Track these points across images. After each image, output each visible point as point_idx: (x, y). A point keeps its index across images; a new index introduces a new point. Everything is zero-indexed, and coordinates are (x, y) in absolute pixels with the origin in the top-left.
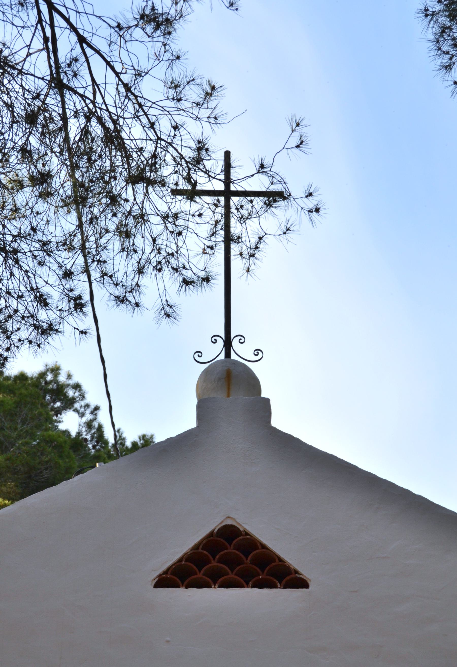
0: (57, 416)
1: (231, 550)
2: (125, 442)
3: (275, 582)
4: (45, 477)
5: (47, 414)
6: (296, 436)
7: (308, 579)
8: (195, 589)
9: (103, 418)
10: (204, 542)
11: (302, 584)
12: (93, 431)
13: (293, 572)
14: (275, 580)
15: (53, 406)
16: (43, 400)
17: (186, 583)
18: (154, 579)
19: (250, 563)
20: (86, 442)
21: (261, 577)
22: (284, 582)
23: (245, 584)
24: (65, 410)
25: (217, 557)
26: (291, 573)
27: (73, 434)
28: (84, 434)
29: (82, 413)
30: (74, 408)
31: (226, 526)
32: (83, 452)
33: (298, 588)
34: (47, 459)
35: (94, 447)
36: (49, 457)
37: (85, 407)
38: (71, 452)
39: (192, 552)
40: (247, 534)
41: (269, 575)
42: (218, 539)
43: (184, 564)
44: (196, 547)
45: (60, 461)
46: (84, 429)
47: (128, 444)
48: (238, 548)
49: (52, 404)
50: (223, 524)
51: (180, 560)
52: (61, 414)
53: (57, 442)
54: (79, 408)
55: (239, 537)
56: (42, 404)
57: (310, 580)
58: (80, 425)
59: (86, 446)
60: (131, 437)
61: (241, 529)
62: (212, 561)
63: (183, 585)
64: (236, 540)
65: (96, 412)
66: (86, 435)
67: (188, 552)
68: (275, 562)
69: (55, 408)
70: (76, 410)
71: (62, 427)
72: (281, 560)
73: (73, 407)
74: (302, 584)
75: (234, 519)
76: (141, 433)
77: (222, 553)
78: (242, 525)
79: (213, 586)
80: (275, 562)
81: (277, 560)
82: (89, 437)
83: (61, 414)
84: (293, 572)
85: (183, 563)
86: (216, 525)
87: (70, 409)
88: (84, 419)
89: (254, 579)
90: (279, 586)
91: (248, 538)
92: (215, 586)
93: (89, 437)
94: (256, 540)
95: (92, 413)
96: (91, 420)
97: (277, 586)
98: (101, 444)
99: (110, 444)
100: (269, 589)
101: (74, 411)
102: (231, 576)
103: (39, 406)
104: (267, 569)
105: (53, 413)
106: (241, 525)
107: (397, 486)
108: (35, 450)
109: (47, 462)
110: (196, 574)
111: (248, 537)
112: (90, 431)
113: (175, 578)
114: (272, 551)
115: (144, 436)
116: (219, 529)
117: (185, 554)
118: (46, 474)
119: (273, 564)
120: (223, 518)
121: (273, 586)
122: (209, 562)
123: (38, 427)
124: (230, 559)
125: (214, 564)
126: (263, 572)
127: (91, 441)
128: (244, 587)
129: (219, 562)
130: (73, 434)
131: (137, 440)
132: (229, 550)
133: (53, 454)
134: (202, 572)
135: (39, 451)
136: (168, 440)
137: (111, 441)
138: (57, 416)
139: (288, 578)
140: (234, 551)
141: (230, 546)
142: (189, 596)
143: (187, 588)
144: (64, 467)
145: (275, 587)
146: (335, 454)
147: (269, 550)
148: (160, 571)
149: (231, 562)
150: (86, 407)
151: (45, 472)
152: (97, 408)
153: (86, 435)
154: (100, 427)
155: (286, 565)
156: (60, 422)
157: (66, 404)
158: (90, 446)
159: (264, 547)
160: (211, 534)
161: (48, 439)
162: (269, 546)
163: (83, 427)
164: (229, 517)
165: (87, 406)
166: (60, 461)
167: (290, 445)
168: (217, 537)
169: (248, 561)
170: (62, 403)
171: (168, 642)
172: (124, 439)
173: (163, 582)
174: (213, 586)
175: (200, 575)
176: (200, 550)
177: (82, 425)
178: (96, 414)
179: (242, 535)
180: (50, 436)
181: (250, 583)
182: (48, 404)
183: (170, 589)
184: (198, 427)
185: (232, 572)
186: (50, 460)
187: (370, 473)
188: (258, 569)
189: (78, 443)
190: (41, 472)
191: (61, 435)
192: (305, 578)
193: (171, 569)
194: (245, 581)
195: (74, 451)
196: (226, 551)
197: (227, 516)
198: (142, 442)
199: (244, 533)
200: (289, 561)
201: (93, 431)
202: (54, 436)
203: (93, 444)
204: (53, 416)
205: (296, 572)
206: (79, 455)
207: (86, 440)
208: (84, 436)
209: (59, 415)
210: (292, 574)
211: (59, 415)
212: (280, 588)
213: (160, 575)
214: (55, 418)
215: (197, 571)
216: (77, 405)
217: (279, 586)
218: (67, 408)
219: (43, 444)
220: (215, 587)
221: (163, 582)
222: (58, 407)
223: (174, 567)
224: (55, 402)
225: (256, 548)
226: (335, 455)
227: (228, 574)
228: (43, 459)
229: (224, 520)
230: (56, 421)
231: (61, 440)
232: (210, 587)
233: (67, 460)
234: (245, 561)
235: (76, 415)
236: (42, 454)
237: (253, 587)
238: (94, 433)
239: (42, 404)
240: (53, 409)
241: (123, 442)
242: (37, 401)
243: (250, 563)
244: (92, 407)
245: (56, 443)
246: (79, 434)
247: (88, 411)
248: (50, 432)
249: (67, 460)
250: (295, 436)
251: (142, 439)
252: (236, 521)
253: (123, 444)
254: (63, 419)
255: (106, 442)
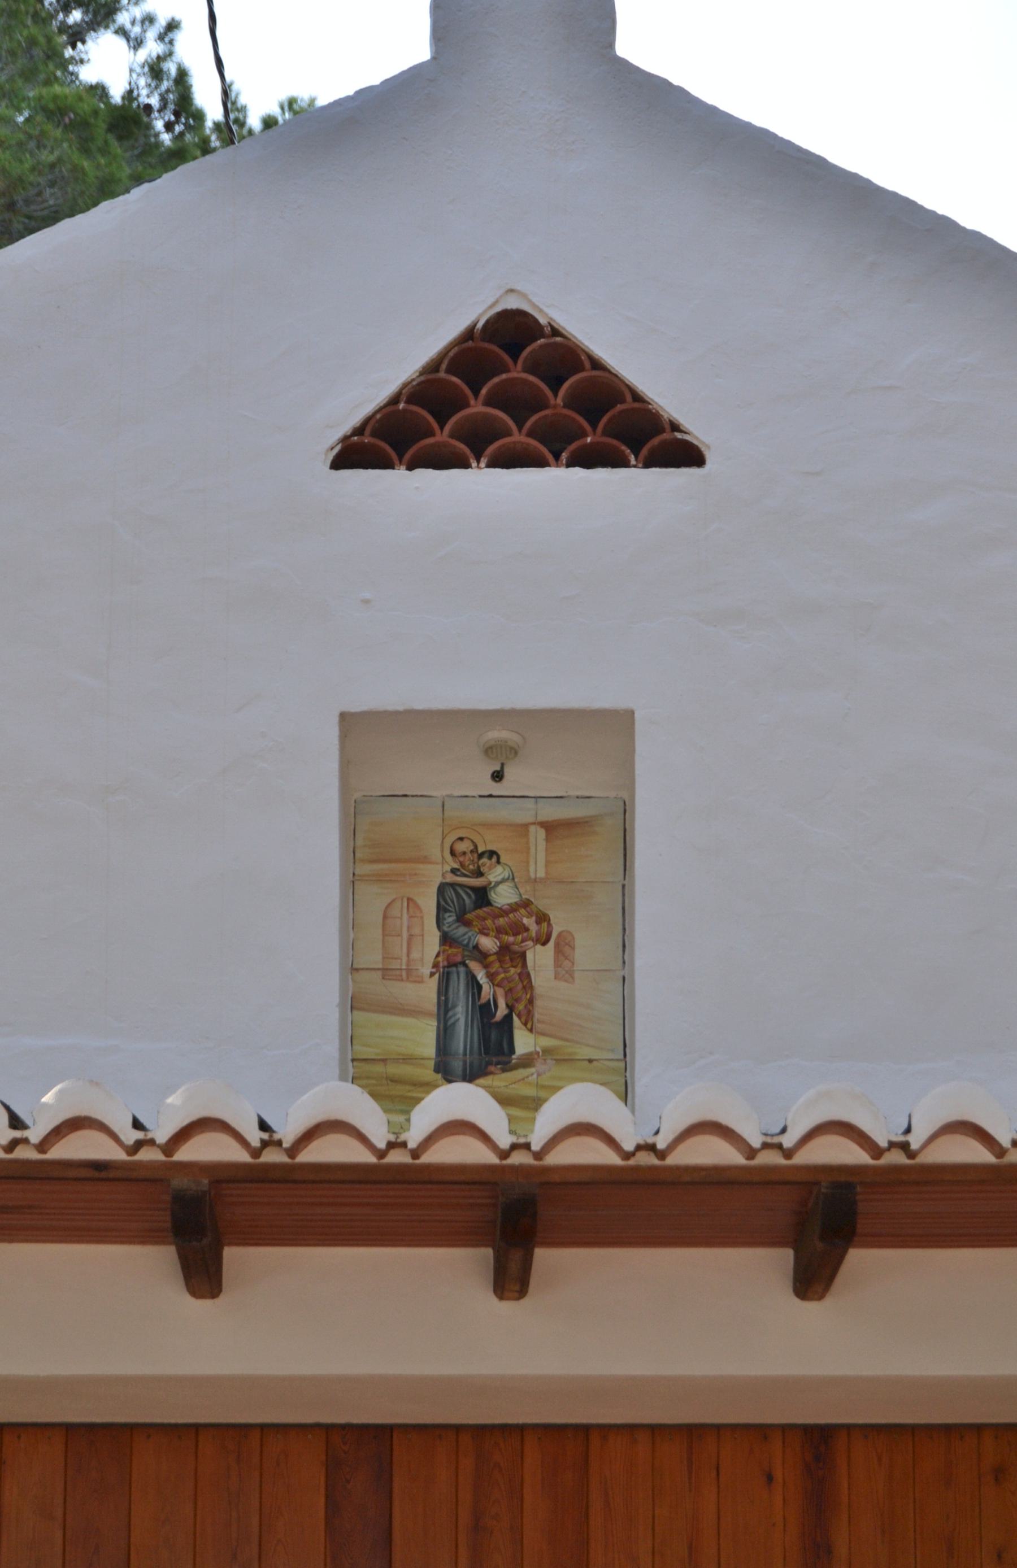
0: (74, 47)
1: (517, 372)
2: (245, 117)
3: (623, 452)
4: (51, 206)
5: (49, 40)
6: (675, 82)
7: (703, 443)
8: (430, 472)
9: (192, 51)
10: (451, 354)
11: (689, 456)
12: (165, 85)
13: (667, 427)
14: (623, 448)
15: (63, 23)
16: (39, 6)
17: (407, 456)
18: (332, 449)
19: (565, 406)
20: (149, 115)
21: (589, 440)
22: (645, 451)
23: (550, 457)
24: (95, 30)
25: (484, 391)
26: (662, 431)
27: (117, 94)
28: (144, 92)
29: (136, 39)
30: (116, 26)
31: (507, 315)
32: (142, 140)
33: (678, 465)
34: (52, 158)
35: (169, 127)
36: (57, 153)
37: (143, 22)
38: (112, 139)
39: (422, 378)
40: (555, 332)
41: (609, 436)
42: (486, 345)
43: (404, 410)
44: (432, 367)
45: (86, 164)
46: (142, 82)
47: (254, 122)
48: (532, 368)
49: (61, 16)
50: (498, 309)
51: (394, 400)
52: (84, 42)
53: (76, 114)
54: (128, 26)
55: (536, 340)
56: (36, 16)
57: (708, 447)
58: (131, 71)
59: (149, 126)
60: (259, 105)
61: (543, 321)
62: (472, 402)
63: (401, 463)
64: (529, 349)
65: (170, 35)
66: (148, 96)
67: (413, 380)
68: (623, 401)
69: (70, 27)
70: (121, 31)
71: (87, 75)
72: (637, 397)
73: (114, 21)
74: (689, 456)
75: (524, 296)
76: (284, 96)
77: (496, 380)
78: (546, 310)
79: (474, 464)
80: (623, 401)
81: (629, 397)
82: (154, 101)
83: (84, 42)
84: (667, 427)
85: (401, 406)
86: (480, 311)
87: (107, 27)
88: (142, 55)
89: (573, 446)
90: (633, 462)
91: (556, 344)
92: (478, 462)
93: (154, 101)
94: (578, 346)
95: (161, 38)
96: (159, 57)
97: (629, 461)
98: (187, 119)
99: (209, 124)
100: (609, 470)
101: (116, 32)
102: (518, 438)
103: (29, 22)
104: (605, 419)
105: (65, 38)
106: (541, 311)
107: (921, 208)
108: (21, 136)
109: (52, 166)
110: (432, 434)
111: (558, 339)
112: (156, 88)
113: (383, 444)
114: (616, 376)
115: (292, 102)
116: (487, 322)
117: (405, 385)
118: (51, 198)
119: (620, 407)
120: (498, 294)
121: (617, 462)
122: (467, 405)
123: (29, 75)
124: (517, 395)
125: (477, 408)
126: (594, 427)
127: (160, 111)
128: (549, 466)
129: (488, 402)
130: (117, 94)
131: (275, 110)
132: (513, 374)
133: (65, 145)
134: (520, 361)
135: (30, 137)
136: (359, 93)
137: (214, 113)
138: (74, 47)
139: (656, 441)
140: (524, 375)
141: (515, 362)
142: (417, 488)
143: (410, 468)
144: (97, 178)
145: (624, 464)
146: (772, 129)
147: (610, 372)
148: (346, 427)
149: (518, 404)
150: (147, 23)
151: (48, 191)
152: (172, 26)
153: (148, 96)
154: (182, 76)
155: (650, 411)
156: (82, 61)
157: (95, 14)
158: (159, 125)
159: (597, 364)
160: (469, 334)
161: (51, 106)
162: (609, 361)
163: (139, 75)
164: (512, 291)
165: (149, 19)
166: (86, 164)
167: (659, 103)
168: (483, 340)
169: (559, 401)
170: (85, 13)
171: (366, 602)
172: (243, 109)
173: (351, 455)
174: (474, 464)
175: (442, 436)
176: (442, 374)
177: (138, 70)
178: (171, 42)
179: (543, 336)
180: (55, 98)
181: (564, 456)
182: (52, 16)
183: (370, 472)
184: (434, 58)
185: (520, 430)
186: (60, 160)
187: (855, 177)
188: (581, 420)
189: (127, 119)
190: (40, 194)
191: (84, 95)
192: (695, 442)
193: (372, 423)
194: (551, 451)
195: (120, 138)
196: (504, 376)
197: (509, 287)
198: (287, 115)
199: (548, 330)
200: (656, 400)
201: (165, 85)
202: (66, 97)
203: (167, 118)
204: (65, 47)
205: (675, 427)
206: (133, 147)
207: (148, 108)
208: (144, 100)
209: (79, 44)
210: (663, 431)
211: (79, 44)
212: (635, 466)
213: (345, 439)
214: (69, 52)
215: (435, 425)
216: (123, 18)
217: (633, 462)
218: (99, 24)
219: (40, 118)
220: (478, 467)
221: (351, 455)
222: (76, 24)
223: (378, 416)
224: (67, 9)
225: (578, 368)
226: (772, 130)
227: (509, 434)
228: (43, 157)
229: (501, 297)
230: (72, 60)
231: (85, 107)
232: (466, 466)
233: (102, 161)
234: (552, 402)
235: (120, 43)
236: (40, 146)
237: (570, 464)
238: (168, 91)
239: (36, 16)
240: (64, 28)
241: (241, 117)
242: (22, 7)
243: (565, 406)
244: (162, 22)
245: (72, 116)
246: (130, 95)
247: (151, 34)
248: (57, 89)
249: (102, 161)
250: (675, 83)
251: (286, 108)
252: (530, 301)
253: (241, 123)
254: (90, 56)
255: (199, 116)
